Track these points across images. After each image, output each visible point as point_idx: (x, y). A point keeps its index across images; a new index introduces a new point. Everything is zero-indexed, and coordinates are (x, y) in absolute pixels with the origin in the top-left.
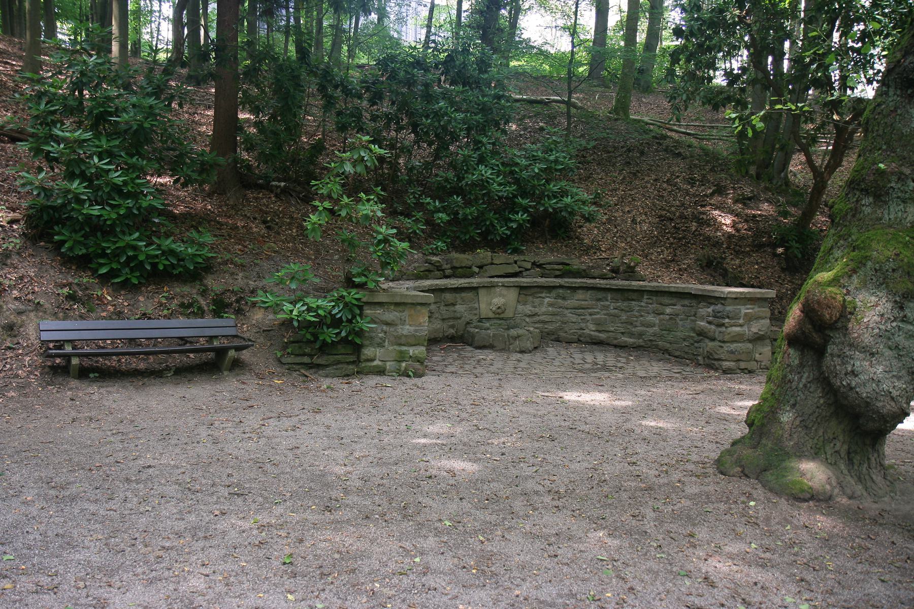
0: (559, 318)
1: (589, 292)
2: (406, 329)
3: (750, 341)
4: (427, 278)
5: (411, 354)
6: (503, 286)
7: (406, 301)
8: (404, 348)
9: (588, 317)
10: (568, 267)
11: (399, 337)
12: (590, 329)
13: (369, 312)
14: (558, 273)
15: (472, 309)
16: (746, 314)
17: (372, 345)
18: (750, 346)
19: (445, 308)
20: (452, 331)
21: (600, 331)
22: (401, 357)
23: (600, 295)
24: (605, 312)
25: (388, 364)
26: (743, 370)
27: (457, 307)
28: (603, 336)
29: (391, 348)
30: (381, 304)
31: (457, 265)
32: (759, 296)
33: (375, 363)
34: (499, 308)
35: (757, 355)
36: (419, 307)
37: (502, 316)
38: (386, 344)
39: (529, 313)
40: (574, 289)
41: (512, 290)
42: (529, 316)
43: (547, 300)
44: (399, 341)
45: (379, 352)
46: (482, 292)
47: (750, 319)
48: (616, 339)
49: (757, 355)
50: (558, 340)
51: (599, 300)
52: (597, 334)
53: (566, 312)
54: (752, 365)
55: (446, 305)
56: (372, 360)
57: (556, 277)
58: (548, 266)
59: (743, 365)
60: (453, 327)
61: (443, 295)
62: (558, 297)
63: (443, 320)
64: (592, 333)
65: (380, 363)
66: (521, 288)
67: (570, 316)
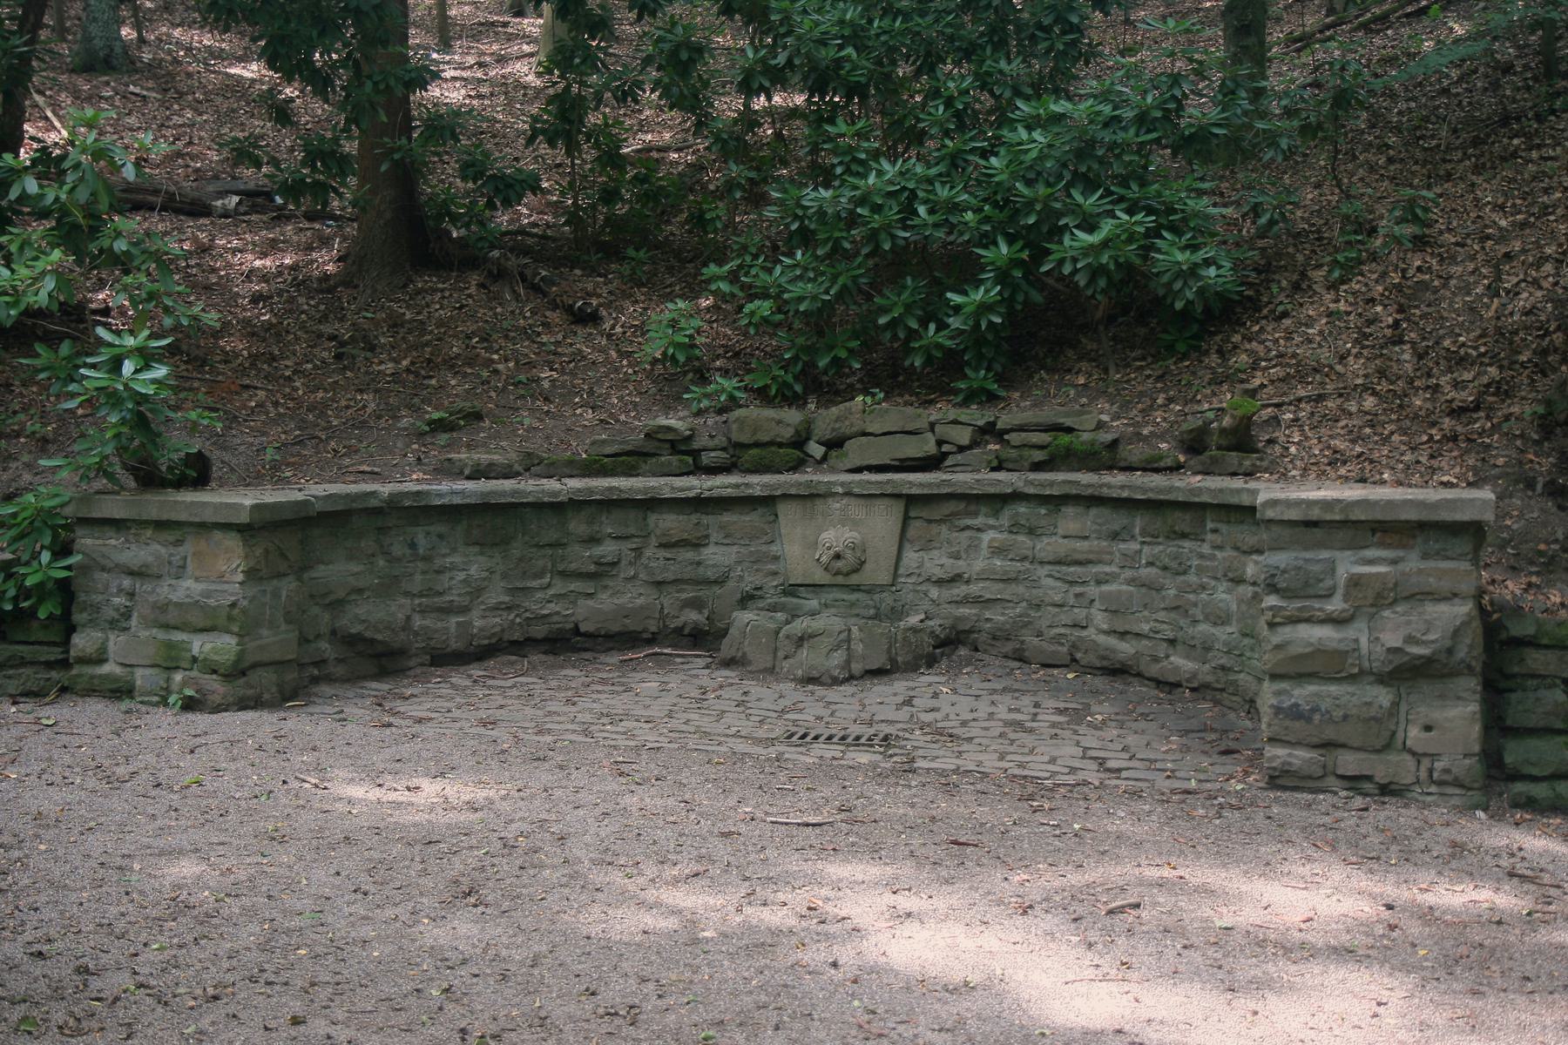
0: (1021, 589)
1: (1094, 511)
2: (188, 588)
3: (1382, 679)
4: (630, 472)
5: (196, 651)
6: (848, 494)
7: (174, 516)
8: (178, 636)
9: (1092, 590)
10: (1065, 439)
11: (163, 608)
12: (1098, 634)
13: (89, 541)
14: (1039, 456)
15: (758, 559)
16: (1355, 582)
17: (93, 623)
18: (1383, 697)
19: (663, 553)
20: (692, 616)
21: (1123, 635)
22: (171, 660)
23: (1117, 520)
24: (1128, 573)
25: (139, 673)
26: (1354, 782)
27: (711, 549)
28: (1126, 648)
29: (144, 634)
30: (117, 524)
31: (744, 438)
32: (1412, 515)
33: (106, 669)
34: (838, 556)
35: (1414, 732)
36: (218, 535)
37: (854, 579)
38: (134, 622)
39: (938, 573)
40: (1056, 502)
41: (881, 504)
42: (940, 582)
43: (987, 537)
44: (167, 618)
45: (115, 642)
46: (786, 511)
47: (1374, 599)
48: (1156, 659)
49: (1414, 732)
50: (1020, 657)
51: (1114, 536)
52: (1112, 641)
53: (1042, 571)
54: (1399, 767)
55: (661, 546)
56: (101, 661)
57: (1037, 467)
58: (1014, 438)
59: (1349, 762)
60: (696, 604)
61: (652, 518)
62: (1014, 528)
63: (659, 584)
64: (1102, 639)
65: (118, 670)
66: (911, 501)
67: (1050, 586)
